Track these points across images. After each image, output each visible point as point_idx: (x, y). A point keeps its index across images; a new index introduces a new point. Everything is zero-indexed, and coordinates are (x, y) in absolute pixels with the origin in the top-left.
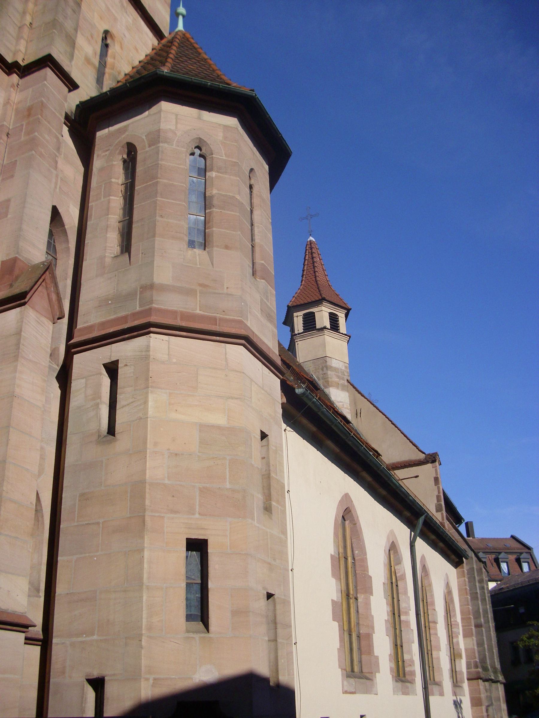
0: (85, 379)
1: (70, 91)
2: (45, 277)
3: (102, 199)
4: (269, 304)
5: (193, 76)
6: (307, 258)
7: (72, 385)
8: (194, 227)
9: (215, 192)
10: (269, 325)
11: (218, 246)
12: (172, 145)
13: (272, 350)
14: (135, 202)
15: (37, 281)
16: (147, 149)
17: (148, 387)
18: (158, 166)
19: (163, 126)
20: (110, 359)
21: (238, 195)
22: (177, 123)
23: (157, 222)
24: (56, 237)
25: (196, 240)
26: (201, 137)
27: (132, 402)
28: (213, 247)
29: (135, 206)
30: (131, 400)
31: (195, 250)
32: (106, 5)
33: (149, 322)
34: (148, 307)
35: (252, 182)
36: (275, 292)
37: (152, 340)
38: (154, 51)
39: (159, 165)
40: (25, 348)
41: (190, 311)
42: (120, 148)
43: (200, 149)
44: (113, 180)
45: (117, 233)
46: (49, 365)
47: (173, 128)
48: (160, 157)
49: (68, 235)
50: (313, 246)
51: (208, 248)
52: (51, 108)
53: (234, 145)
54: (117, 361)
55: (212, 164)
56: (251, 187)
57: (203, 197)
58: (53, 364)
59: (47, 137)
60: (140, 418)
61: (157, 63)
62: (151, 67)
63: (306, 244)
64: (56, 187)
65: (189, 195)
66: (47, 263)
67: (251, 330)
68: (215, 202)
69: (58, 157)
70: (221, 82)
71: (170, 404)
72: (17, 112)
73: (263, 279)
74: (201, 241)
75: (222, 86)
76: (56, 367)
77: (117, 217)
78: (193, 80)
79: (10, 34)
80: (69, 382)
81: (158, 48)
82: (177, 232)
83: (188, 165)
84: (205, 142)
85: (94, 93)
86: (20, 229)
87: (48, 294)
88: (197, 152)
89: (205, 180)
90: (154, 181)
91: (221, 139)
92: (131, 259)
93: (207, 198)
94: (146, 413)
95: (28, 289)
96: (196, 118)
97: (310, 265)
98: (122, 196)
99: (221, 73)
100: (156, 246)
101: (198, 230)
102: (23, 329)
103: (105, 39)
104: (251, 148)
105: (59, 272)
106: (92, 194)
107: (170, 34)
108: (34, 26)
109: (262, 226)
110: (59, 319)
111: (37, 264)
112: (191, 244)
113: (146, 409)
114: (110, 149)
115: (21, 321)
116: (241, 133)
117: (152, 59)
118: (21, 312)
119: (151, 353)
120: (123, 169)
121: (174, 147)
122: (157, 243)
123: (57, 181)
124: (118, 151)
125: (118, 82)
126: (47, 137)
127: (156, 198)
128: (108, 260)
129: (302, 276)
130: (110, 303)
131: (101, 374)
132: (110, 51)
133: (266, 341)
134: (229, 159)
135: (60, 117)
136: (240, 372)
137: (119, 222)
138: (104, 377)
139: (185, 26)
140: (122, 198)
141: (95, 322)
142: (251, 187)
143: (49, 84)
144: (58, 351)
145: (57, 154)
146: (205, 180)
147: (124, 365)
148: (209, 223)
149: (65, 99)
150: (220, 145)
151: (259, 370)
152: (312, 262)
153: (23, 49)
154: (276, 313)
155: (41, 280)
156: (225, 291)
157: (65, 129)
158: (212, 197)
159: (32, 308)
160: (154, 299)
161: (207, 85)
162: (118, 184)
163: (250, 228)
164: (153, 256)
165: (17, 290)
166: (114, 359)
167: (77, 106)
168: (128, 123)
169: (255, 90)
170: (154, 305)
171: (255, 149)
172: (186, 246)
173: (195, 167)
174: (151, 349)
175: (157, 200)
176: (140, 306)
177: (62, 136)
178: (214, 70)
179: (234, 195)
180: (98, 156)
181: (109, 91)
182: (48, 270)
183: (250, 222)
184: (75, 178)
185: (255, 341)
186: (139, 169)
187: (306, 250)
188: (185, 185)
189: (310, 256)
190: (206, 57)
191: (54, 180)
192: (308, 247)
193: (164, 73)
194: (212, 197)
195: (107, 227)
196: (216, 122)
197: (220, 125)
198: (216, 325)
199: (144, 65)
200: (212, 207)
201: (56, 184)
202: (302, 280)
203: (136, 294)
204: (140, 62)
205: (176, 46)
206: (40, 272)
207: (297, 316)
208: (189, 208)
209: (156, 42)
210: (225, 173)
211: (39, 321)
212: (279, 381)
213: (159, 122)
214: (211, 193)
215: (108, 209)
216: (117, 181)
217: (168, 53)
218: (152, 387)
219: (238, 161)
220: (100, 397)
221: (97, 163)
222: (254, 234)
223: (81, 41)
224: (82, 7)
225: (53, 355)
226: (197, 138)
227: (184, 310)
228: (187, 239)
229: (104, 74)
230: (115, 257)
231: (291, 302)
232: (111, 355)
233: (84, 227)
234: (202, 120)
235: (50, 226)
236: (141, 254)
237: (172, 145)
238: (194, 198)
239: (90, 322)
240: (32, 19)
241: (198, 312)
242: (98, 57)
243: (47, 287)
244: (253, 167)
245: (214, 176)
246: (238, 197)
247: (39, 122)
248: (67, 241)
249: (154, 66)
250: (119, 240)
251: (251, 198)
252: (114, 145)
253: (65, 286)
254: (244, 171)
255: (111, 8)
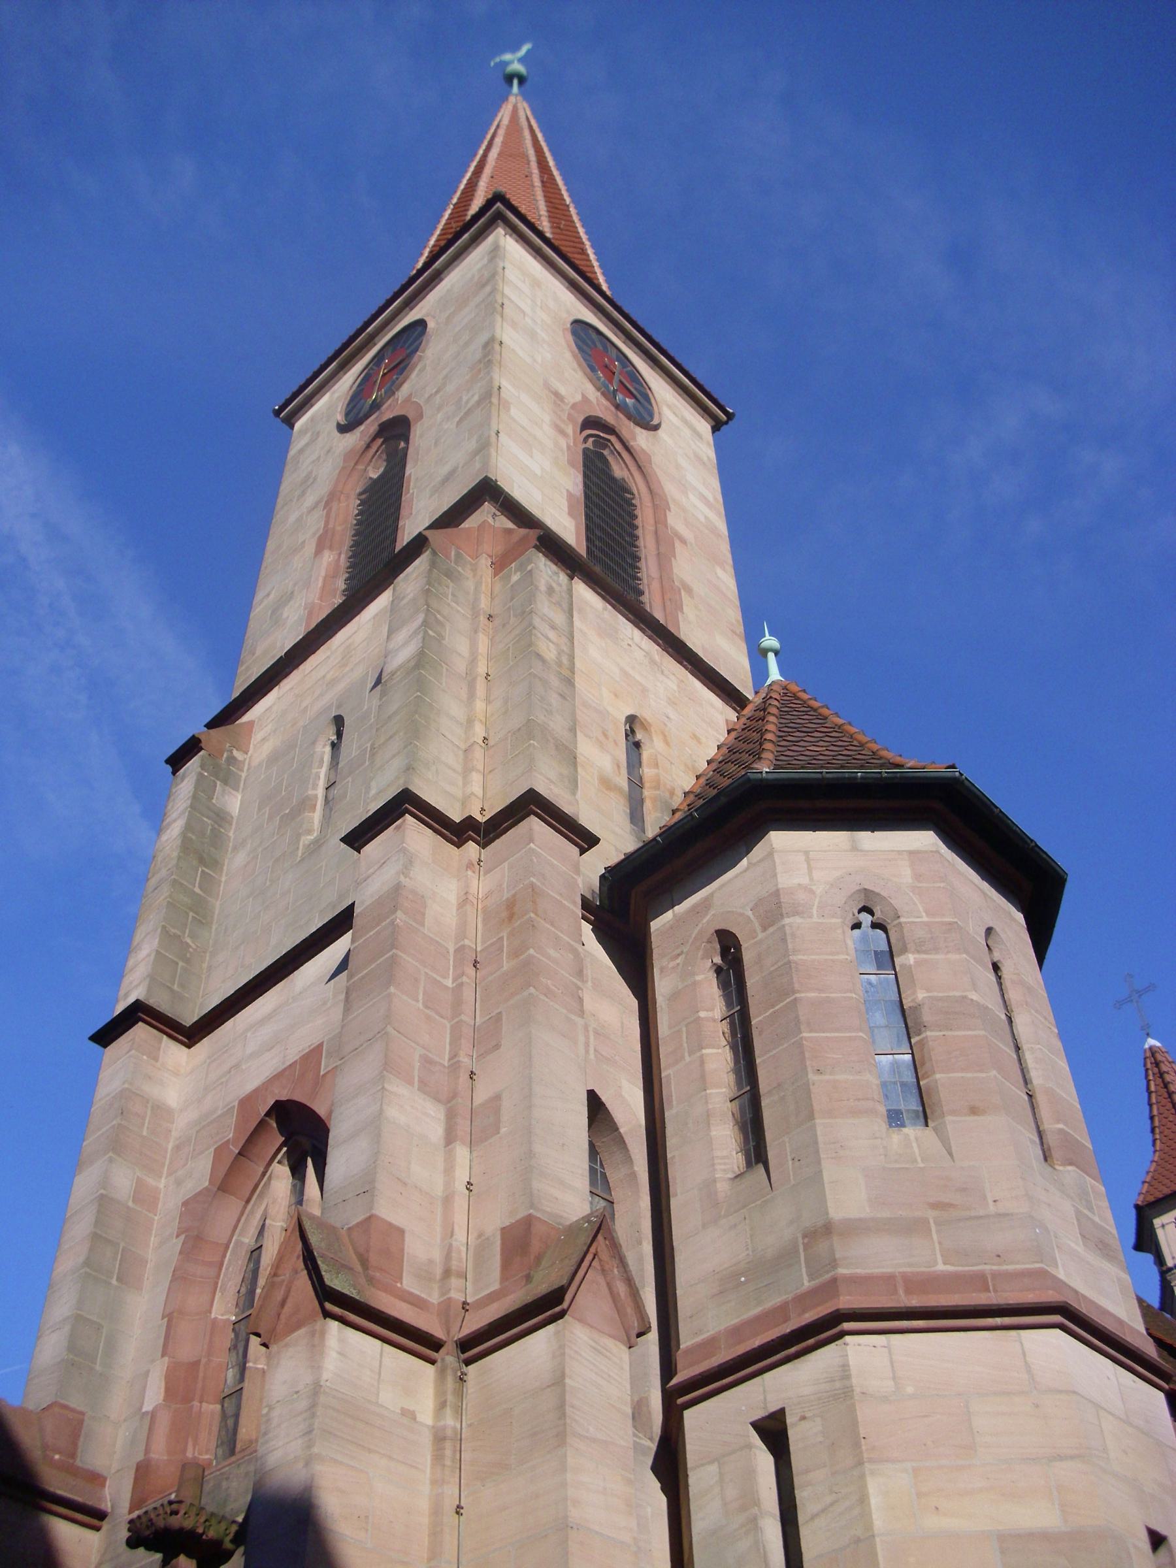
0: (716, 1463)
1: (583, 851)
2: (597, 1249)
3: (687, 1059)
4: (1097, 1219)
5: (822, 767)
6: (1153, 1088)
7: (691, 1481)
8: (893, 1080)
9: (921, 995)
10: (1107, 1266)
11: (954, 1112)
12: (811, 917)
13: (1129, 1325)
14: (757, 1052)
15: (582, 1260)
16: (761, 936)
17: (860, 1463)
18: (790, 966)
19: (785, 881)
20: (765, 1408)
21: (974, 992)
22: (810, 869)
23: (811, 1087)
24: (604, 1155)
25: (902, 1107)
26: (866, 887)
27: (832, 1504)
28: (943, 1115)
29: (758, 1061)
30: (829, 1499)
31: (905, 1130)
32: (622, 669)
33: (838, 1310)
34: (827, 1277)
35: (997, 956)
36: (1103, 1189)
37: (850, 1350)
38: (734, 734)
39: (793, 965)
40: (578, 1413)
41: (923, 1269)
42: (704, 944)
43: (871, 913)
44: (702, 1014)
45: (732, 1124)
46: (634, 1441)
47: (805, 880)
48: (790, 946)
49: (630, 1148)
50: (1159, 1057)
51: (933, 1121)
52: (551, 893)
53: (940, 887)
54: (782, 1412)
55: (903, 938)
56: (996, 967)
57: (898, 1012)
58: (640, 1438)
59: (552, 952)
60: (858, 1540)
61: (745, 756)
62: (732, 768)
63: (1143, 1057)
64: (587, 1052)
65: (868, 1014)
66: (597, 1217)
67: (1070, 1286)
68: (927, 1017)
69: (582, 990)
70: (882, 766)
71: (919, 1495)
72: (487, 915)
73: (1071, 1164)
74: (914, 1108)
75: (886, 772)
76: (648, 1443)
77: (724, 1090)
78: (824, 774)
79: (450, 768)
80: (681, 1476)
81: (740, 726)
82: (859, 1100)
83: (852, 952)
84: (878, 894)
85: (630, 845)
86: (530, 1154)
87: (609, 1286)
88: (866, 919)
89: (896, 975)
90: (788, 1000)
91: (910, 881)
92: (772, 1175)
93: (907, 1013)
94: (869, 1527)
95: (564, 1282)
96: (847, 851)
97: (1164, 1102)
98: (726, 1043)
99: (879, 747)
100: (820, 1139)
101: (903, 1084)
102: (567, 1371)
103: (630, 733)
104: (976, 885)
105: (621, 1227)
106: (665, 1051)
107: (756, 693)
108: (491, 742)
109: (1039, 1046)
110: (639, 1335)
111: (576, 1221)
112: (895, 1118)
113: (865, 1516)
114: (685, 951)
115: (560, 1353)
116: (950, 859)
117: (731, 750)
118: (557, 1333)
119: (854, 1381)
120: (719, 987)
121: (815, 919)
122: (819, 1131)
123: (587, 1038)
124: (700, 953)
125: (674, 812)
126: (552, 952)
127: (801, 1035)
128: (723, 1187)
129: (1153, 1131)
130: (746, 1281)
131: (749, 1446)
132: (646, 754)
133: (1111, 1308)
134: (937, 920)
135: (572, 907)
136: (1067, 1392)
137: (731, 1101)
138: (758, 1452)
139: (782, 672)
140: (728, 1047)
141: (717, 1330)
142: (996, 967)
143: (540, 848)
144: (648, 1406)
145: (579, 983)
146: (896, 975)
147: (798, 1418)
148: (923, 1064)
149: (577, 869)
150: (911, 894)
151: (1108, 1378)
152: (1166, 1095)
153: (477, 789)
154: (1117, 1236)
155: (589, 1257)
156: (992, 1208)
157: (587, 928)
158: (917, 1008)
159: (580, 1320)
160: (837, 1256)
161: (856, 778)
162: (714, 1020)
163: (1015, 1056)
164: (818, 1162)
165: (542, 1286)
166: (773, 1408)
167: (602, 877)
168: (710, 891)
169: (957, 766)
170: (842, 1271)
171: (985, 886)
172: (884, 1126)
173: (867, 951)
174: (854, 1371)
175: (802, 1038)
176: (811, 1277)
177: (583, 945)
178: (862, 745)
179: (964, 994)
180: (662, 970)
181: (660, 835)
182: (601, 1231)
183: (1012, 1044)
184: (622, 1023)
185: (1084, 1311)
186: (753, 981)
187: (1147, 1070)
188: (854, 996)
189: (1159, 1081)
190: (840, 721)
191: (581, 1039)
192: (1148, 1061)
193: (764, 775)
194: (917, 1008)
195: (708, 1116)
196: (893, 849)
197: (900, 852)
198: (987, 1290)
199: (719, 766)
200: (923, 1029)
201: (587, 1045)
202: (1154, 1141)
203: (797, 1251)
204: (709, 762)
205: (774, 715)
206: (584, 1239)
207: (1163, 1226)
208: (874, 1042)
209: (732, 715)
210: (936, 950)
211: (599, 1348)
212: (1161, 1396)
213: (775, 875)
214: (913, 1000)
215: (703, 1077)
216: (710, 1014)
217: (762, 732)
218: (871, 1461)
219: (956, 920)
220: (756, 1502)
221: (663, 985)
222: (1027, 1067)
223: (586, 748)
224: (576, 685)
225: (638, 1413)
226: (859, 891)
227: (909, 1270)
228: (882, 1110)
229: (642, 801)
230: (736, 1177)
231: (1142, 1196)
232: (765, 1399)
233: (658, 1125)
234: (861, 851)
235: (589, 1137)
236: (790, 1162)
237: (811, 917)
238: (879, 1018)
239: (708, 1331)
240: (487, 730)
241: (941, 1267)
242: (624, 771)
243: (603, 1270)
244: (991, 925)
245: (912, 961)
246: (974, 996)
247: (533, 926)
248: (629, 1159)
249: (741, 764)
250: (739, 1141)
251: (1001, 990)
252: (691, 940)
253: (641, 1260)
254: (974, 937)
255: (631, 672)
